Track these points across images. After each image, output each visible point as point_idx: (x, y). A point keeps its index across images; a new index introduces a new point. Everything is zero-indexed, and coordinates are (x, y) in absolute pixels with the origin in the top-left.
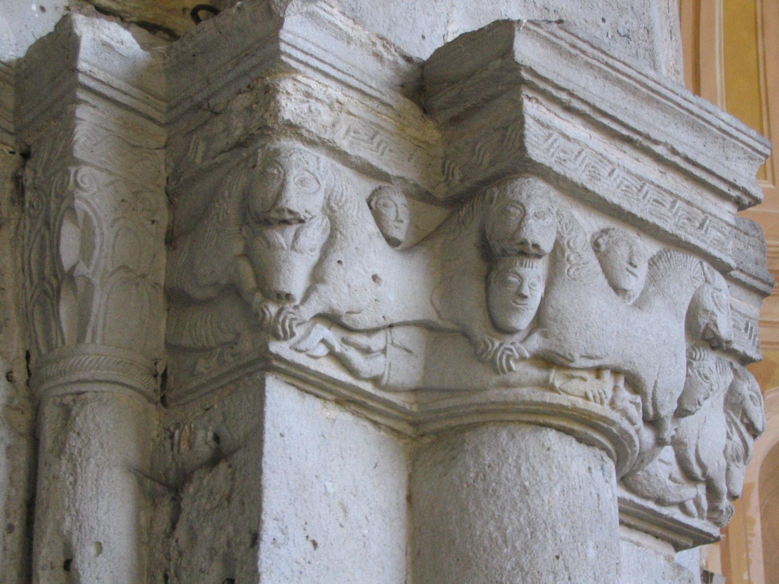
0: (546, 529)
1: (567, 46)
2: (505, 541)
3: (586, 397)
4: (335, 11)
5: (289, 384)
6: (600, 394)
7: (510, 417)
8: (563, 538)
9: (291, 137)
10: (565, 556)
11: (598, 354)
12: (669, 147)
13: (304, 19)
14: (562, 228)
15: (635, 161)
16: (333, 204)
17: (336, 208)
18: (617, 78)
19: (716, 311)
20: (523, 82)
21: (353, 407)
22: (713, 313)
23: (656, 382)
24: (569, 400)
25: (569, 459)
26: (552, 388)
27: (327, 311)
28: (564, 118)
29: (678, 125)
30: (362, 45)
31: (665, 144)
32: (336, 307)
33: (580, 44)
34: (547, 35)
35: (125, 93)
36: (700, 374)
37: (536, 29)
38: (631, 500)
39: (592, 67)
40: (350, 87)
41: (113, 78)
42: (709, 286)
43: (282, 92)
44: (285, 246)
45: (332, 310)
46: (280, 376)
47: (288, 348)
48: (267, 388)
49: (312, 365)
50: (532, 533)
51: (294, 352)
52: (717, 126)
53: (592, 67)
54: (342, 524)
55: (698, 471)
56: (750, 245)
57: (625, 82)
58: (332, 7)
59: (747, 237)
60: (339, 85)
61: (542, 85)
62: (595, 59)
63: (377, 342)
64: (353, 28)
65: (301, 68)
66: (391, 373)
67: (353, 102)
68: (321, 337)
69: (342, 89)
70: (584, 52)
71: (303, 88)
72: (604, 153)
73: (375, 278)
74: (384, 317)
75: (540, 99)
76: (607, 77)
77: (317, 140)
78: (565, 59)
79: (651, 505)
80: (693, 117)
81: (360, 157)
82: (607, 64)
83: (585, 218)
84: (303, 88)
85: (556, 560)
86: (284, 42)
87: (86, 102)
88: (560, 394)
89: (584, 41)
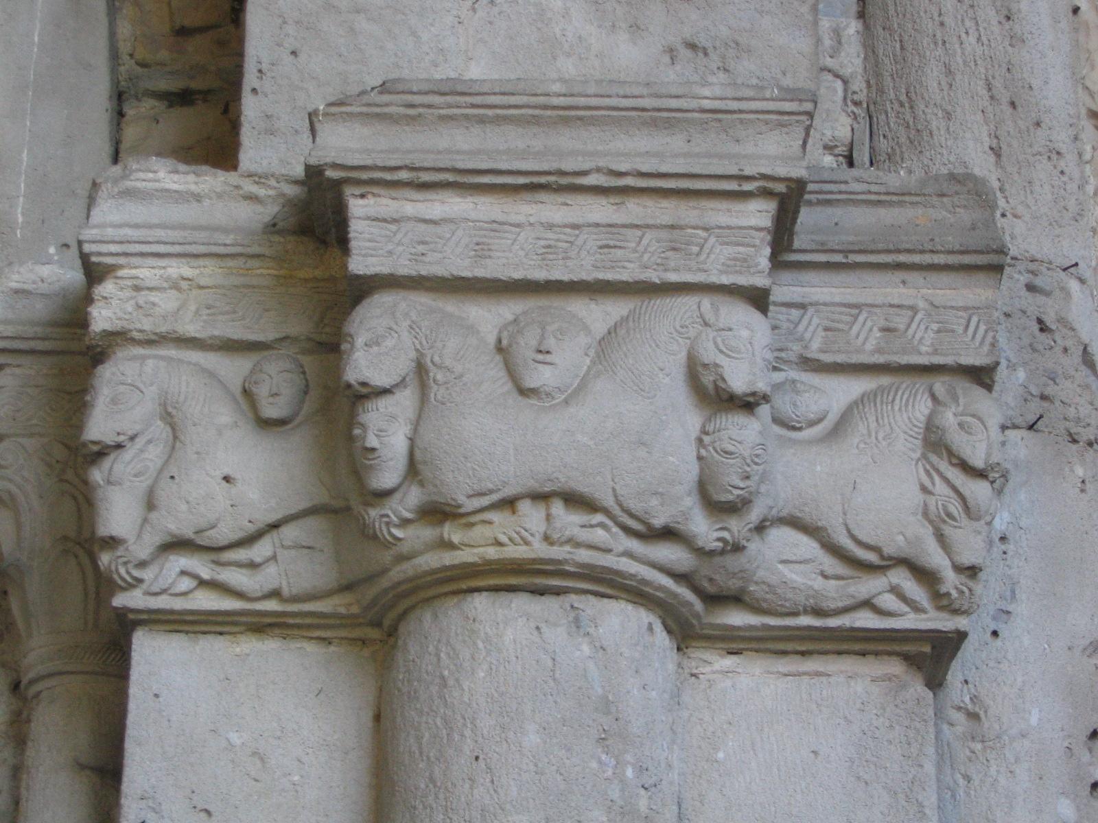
0: (465, 725)
1: (402, 110)
2: (421, 753)
3: (499, 544)
4: (161, 174)
5: (170, 631)
6: (518, 533)
7: (431, 593)
8: (485, 732)
9: (124, 345)
10: (487, 754)
11: (491, 486)
12: (605, 171)
13: (121, 201)
14: (421, 343)
15: (562, 207)
16: (170, 409)
17: (174, 412)
18: (498, 116)
19: (721, 360)
20: (338, 184)
21: (277, 631)
22: (717, 365)
23: (614, 490)
24: (474, 554)
25: (501, 626)
26: (451, 546)
27: (168, 539)
28: (422, 199)
29: (630, 133)
30: (220, 196)
31: (598, 170)
32: (177, 532)
33: (418, 99)
34: (365, 109)
35: (43, 339)
36: (716, 451)
37: (343, 109)
38: (763, 625)
39: (451, 118)
40: (196, 256)
41: (26, 328)
42: (709, 330)
43: (98, 300)
44: (101, 482)
45: (174, 536)
46: (156, 627)
47: (141, 595)
48: (133, 646)
49: (178, 604)
50: (448, 735)
51: (148, 598)
52: (698, 109)
53: (451, 118)
54: (257, 778)
55: (871, 557)
56: (958, 207)
57: (513, 115)
58: (155, 172)
59: (945, 200)
60: (183, 260)
61: (365, 176)
62: (453, 107)
63: (260, 551)
64: (196, 183)
65: (122, 261)
66: (291, 581)
67: (208, 272)
68: (178, 570)
69: (188, 263)
70: (430, 106)
71: (129, 283)
72: (501, 218)
73: (227, 479)
74: (250, 522)
75: (376, 190)
76: (482, 120)
77: (153, 337)
78: (408, 125)
79: (805, 621)
80: (649, 113)
81: (216, 337)
82: (473, 106)
83: (490, 311)
84: (129, 283)
85: (474, 762)
86: (86, 242)
87: (9, 365)
88: (462, 550)
89: (426, 93)
